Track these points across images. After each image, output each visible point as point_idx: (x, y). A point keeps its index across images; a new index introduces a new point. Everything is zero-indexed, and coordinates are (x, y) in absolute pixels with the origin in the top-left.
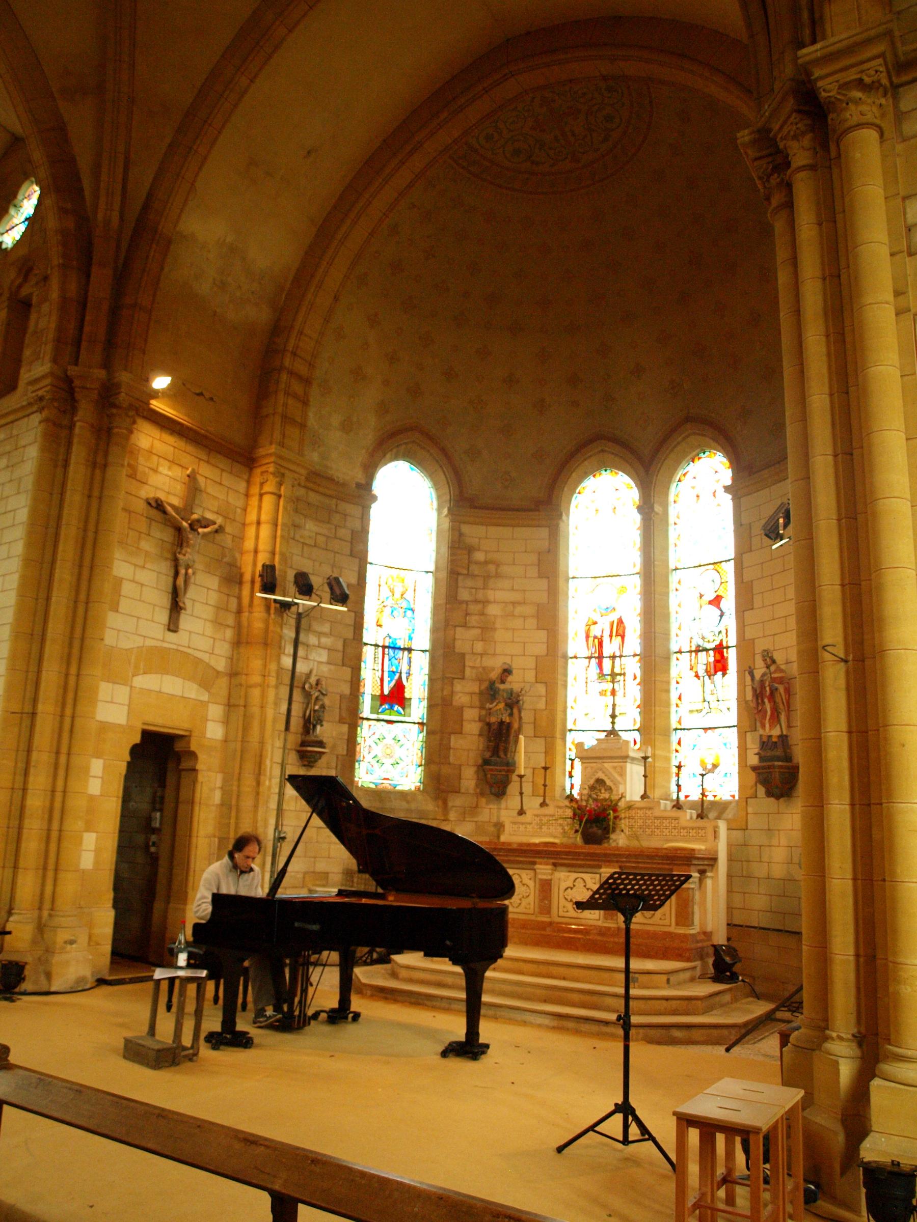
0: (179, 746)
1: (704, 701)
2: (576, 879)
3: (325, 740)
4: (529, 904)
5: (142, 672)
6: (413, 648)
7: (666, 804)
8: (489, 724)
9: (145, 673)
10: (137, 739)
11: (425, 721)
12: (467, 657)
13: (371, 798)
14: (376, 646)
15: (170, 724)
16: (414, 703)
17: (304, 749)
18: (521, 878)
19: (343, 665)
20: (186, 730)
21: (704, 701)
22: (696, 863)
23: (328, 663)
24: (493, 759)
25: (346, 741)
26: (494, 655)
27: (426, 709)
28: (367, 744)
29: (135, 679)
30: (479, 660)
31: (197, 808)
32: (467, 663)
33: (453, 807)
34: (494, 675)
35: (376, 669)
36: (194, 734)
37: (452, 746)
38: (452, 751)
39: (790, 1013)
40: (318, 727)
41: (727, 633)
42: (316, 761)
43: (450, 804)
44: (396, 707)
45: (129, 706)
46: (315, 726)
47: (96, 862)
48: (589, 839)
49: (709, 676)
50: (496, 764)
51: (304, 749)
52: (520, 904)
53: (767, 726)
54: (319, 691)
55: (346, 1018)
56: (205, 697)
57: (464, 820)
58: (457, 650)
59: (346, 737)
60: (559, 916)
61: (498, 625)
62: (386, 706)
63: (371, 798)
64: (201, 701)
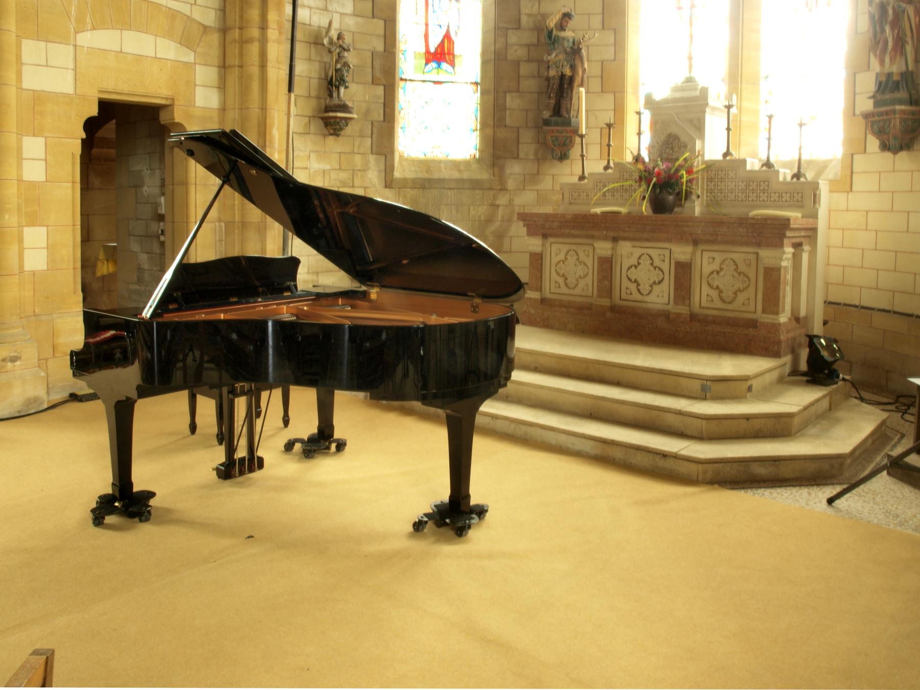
0: (164, 118)
2: (641, 256)
3: (350, 104)
4: (587, 285)
5: (89, 26)
7: (753, 163)
8: (548, 79)
9: (94, 29)
10: (94, 111)
13: (417, 169)
15: (142, 91)
17: (327, 115)
18: (577, 255)
19: (373, 17)
20: (167, 99)
23: (355, 15)
24: (551, 118)
25: (382, 105)
29: (79, 36)
31: (192, 189)
33: (511, 174)
34: (552, 23)
36: (176, 103)
38: (507, 112)
39: (900, 414)
40: (342, 90)
42: (341, 129)
45: (75, 70)
46: (338, 88)
47: (51, 260)
48: (659, 206)
50: (556, 124)
51: (327, 115)
53: (887, 59)
54: (340, 46)
55: (328, 448)
56: (190, 57)
57: (524, 189)
59: (382, 101)
63: (417, 169)
64: (185, 63)
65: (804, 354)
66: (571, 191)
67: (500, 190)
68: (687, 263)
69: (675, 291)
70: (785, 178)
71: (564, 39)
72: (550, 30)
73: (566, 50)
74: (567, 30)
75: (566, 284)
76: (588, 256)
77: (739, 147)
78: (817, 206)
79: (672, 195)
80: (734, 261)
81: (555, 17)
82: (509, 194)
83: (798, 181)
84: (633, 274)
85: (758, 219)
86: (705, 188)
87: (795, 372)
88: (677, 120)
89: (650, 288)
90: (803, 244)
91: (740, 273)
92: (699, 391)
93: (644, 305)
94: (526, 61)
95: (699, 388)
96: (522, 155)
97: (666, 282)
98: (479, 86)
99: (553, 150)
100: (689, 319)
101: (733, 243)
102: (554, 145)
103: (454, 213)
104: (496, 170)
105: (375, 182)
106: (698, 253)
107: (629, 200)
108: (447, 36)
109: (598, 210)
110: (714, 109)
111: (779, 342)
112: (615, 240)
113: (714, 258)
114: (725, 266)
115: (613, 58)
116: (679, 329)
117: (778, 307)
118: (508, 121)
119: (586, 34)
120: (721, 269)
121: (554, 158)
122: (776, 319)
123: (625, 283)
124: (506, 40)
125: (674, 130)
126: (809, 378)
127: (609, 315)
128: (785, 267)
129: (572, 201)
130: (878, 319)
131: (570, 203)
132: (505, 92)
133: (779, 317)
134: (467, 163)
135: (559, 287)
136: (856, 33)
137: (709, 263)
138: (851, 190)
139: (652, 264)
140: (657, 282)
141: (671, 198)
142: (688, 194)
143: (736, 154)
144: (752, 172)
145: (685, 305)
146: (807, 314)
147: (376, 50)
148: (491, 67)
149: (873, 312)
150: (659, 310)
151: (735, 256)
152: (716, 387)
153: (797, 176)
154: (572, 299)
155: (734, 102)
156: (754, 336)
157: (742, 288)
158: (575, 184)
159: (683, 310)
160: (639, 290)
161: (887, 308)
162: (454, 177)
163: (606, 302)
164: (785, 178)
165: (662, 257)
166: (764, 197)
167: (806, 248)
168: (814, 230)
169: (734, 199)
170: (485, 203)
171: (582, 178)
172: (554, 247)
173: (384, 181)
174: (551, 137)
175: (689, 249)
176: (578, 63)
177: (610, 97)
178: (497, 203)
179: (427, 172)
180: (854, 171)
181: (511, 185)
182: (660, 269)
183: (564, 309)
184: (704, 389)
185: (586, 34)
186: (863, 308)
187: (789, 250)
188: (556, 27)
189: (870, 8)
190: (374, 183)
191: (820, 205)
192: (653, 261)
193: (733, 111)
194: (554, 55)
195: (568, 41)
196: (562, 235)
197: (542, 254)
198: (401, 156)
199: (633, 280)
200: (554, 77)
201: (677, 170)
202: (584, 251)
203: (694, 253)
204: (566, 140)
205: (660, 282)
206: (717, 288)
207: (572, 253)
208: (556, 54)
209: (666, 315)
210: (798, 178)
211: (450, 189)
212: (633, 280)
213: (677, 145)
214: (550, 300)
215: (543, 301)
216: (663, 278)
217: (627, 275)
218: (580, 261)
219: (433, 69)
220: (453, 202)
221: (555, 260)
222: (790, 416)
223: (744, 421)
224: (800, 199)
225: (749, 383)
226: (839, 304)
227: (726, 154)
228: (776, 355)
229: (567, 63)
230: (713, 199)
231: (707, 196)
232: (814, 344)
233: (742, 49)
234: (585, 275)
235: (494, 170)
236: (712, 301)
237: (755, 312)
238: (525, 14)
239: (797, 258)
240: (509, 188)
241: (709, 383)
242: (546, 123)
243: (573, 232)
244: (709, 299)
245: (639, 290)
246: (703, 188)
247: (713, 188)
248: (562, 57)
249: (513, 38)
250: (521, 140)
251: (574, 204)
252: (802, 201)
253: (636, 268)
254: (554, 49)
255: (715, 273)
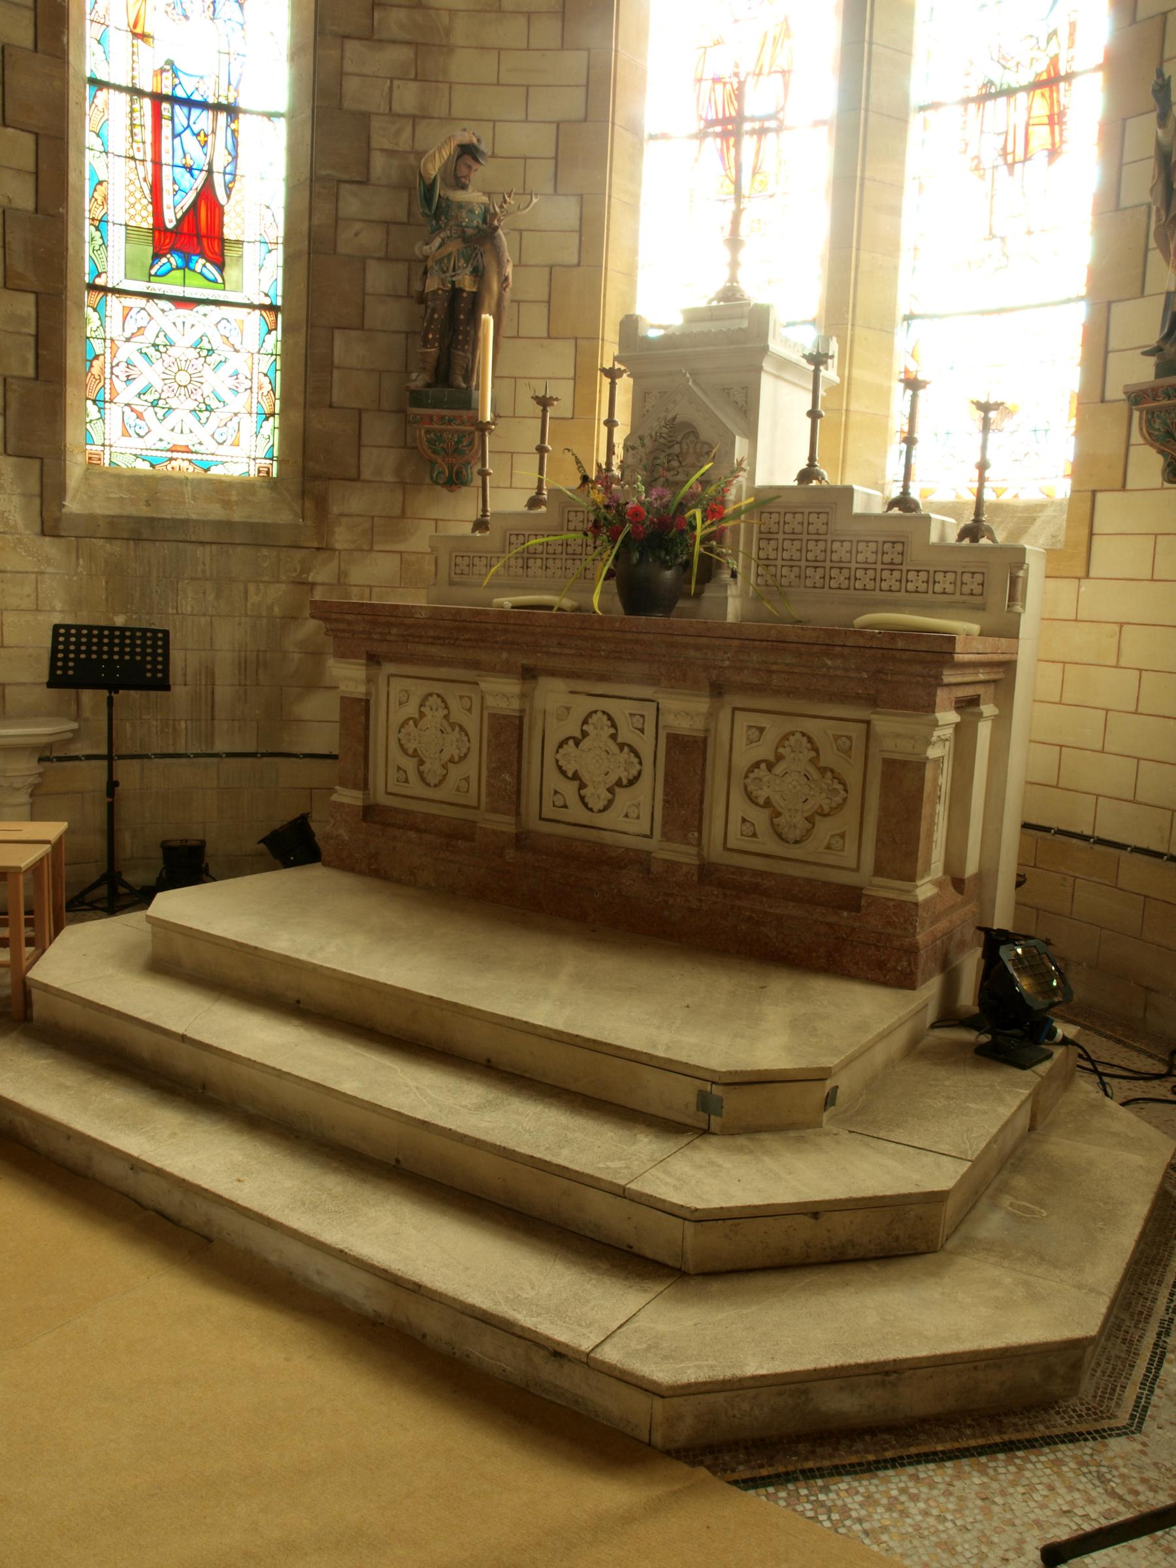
1: (992, 236)
4: (467, 779)
6: (242, 104)
8: (422, 298)
11: (279, 302)
12: (375, 123)
14: (135, 92)
16: (251, 254)
21: (992, 236)
22: (953, 680)
24: (431, 391)
25: (32, 340)
26: (449, 119)
27: (280, 270)
28: (121, 356)
30: (409, 129)
32: (374, 145)
34: (433, 168)
35: (139, 156)
37: (336, 362)
38: (336, 373)
41: (1072, 34)
43: (335, 509)
44: (199, 263)
49: (1011, 167)
52: (444, 777)
57: (371, 550)
58: (346, 105)
60: (541, 818)
61: (458, 38)
62: (175, 260)
65: (971, 965)
66: (454, 554)
67: (318, 549)
68: (694, 740)
69: (664, 807)
70: (943, 536)
71: (460, 206)
72: (429, 182)
73: (464, 232)
74: (470, 188)
75: (421, 774)
76: (470, 710)
77: (843, 468)
78: (1018, 608)
79: (669, 568)
80: (810, 740)
81: (440, 153)
82: (336, 561)
83: (975, 545)
84: (572, 759)
85: (873, 637)
86: (754, 556)
87: (948, 1017)
88: (695, 388)
89: (610, 796)
90: (981, 701)
91: (823, 770)
92: (693, 1108)
93: (593, 835)
94: (379, 259)
95: (692, 1098)
96: (367, 474)
97: (645, 783)
98: (280, 317)
99: (432, 463)
100: (695, 878)
101: (810, 694)
102: (434, 452)
103: (211, 597)
104: (309, 504)
105: (15, 521)
106: (725, 714)
107: (486, 575)
108: (206, 194)
109: (507, 601)
110: (784, 364)
111: (912, 951)
112: (529, 674)
113: (761, 730)
114: (788, 750)
115: (575, 261)
116: (671, 901)
117: (916, 861)
118: (337, 396)
119: (509, 196)
120: (779, 758)
121: (436, 483)
122: (908, 892)
123: (554, 780)
124: (337, 209)
125: (684, 411)
126: (985, 1038)
127: (511, 854)
128: (938, 761)
129: (457, 578)
130: (1134, 872)
131: (452, 583)
132: (333, 328)
133: (917, 887)
134: (244, 487)
135: (407, 781)
136: (1117, 208)
137: (750, 742)
138: (1087, 576)
139: (614, 737)
140: (625, 782)
141: (668, 574)
142: (709, 569)
143: (830, 477)
144: (864, 517)
145: (688, 844)
146: (980, 868)
147: (14, 205)
148: (301, 267)
149: (1123, 853)
150: (628, 849)
151: (811, 726)
152: (733, 1102)
153: (972, 532)
154: (433, 809)
155: (834, 348)
156: (853, 930)
157: (826, 809)
158: (463, 538)
159: (682, 854)
160: (582, 798)
161: (1154, 847)
162: (211, 517)
163: (504, 824)
164: (943, 536)
165: (638, 722)
166: (891, 580)
167: (988, 709)
168: (1008, 666)
169: (819, 583)
170: (283, 578)
171: (481, 524)
172: (397, 685)
173: (39, 520)
174: (428, 432)
175: (701, 705)
176: (489, 261)
177: (567, 348)
178: (310, 579)
179: (148, 504)
180: (1095, 531)
181: (341, 538)
182: (633, 750)
183: (412, 835)
184: (705, 1103)
185: (509, 196)
186: (1101, 842)
187: (948, 717)
188: (443, 179)
189: (1159, 131)
190: (11, 522)
191: (1024, 607)
192: (616, 729)
193: (830, 373)
194: (437, 242)
195: (472, 211)
196: (411, 659)
197: (367, 701)
198: (92, 464)
199: (570, 774)
200: (435, 292)
201: (682, 507)
202: (461, 697)
203: (712, 715)
204: (459, 441)
205: (632, 782)
206: (768, 803)
207: (434, 700)
208: (443, 240)
209: (640, 860)
210: (975, 539)
211: (202, 543)
212: (570, 774)
213: (691, 450)
214: (384, 810)
215: (370, 812)
216: (640, 773)
217: (557, 761)
218: (451, 721)
219: (172, 269)
220: (208, 574)
221: (398, 716)
222: (936, 1198)
223: (809, 1221)
224: (977, 590)
225: (829, 1084)
226: (1047, 830)
227: (806, 475)
228: (906, 981)
229: (467, 262)
230: (770, 582)
231: (758, 575)
232: (999, 959)
233: (858, 249)
234: (462, 755)
235: (303, 504)
236: (754, 835)
237: (857, 870)
238: (382, 150)
239: (964, 736)
240: (337, 546)
241: (717, 1090)
242: (417, 399)
243: (433, 650)
244: (747, 829)
245: (582, 798)
246: (748, 556)
247: (772, 555)
248: (454, 247)
249: (352, 203)
250: (365, 440)
251: (461, 584)
252: (982, 595)
253: (577, 744)
254: (439, 229)
255: (763, 766)
